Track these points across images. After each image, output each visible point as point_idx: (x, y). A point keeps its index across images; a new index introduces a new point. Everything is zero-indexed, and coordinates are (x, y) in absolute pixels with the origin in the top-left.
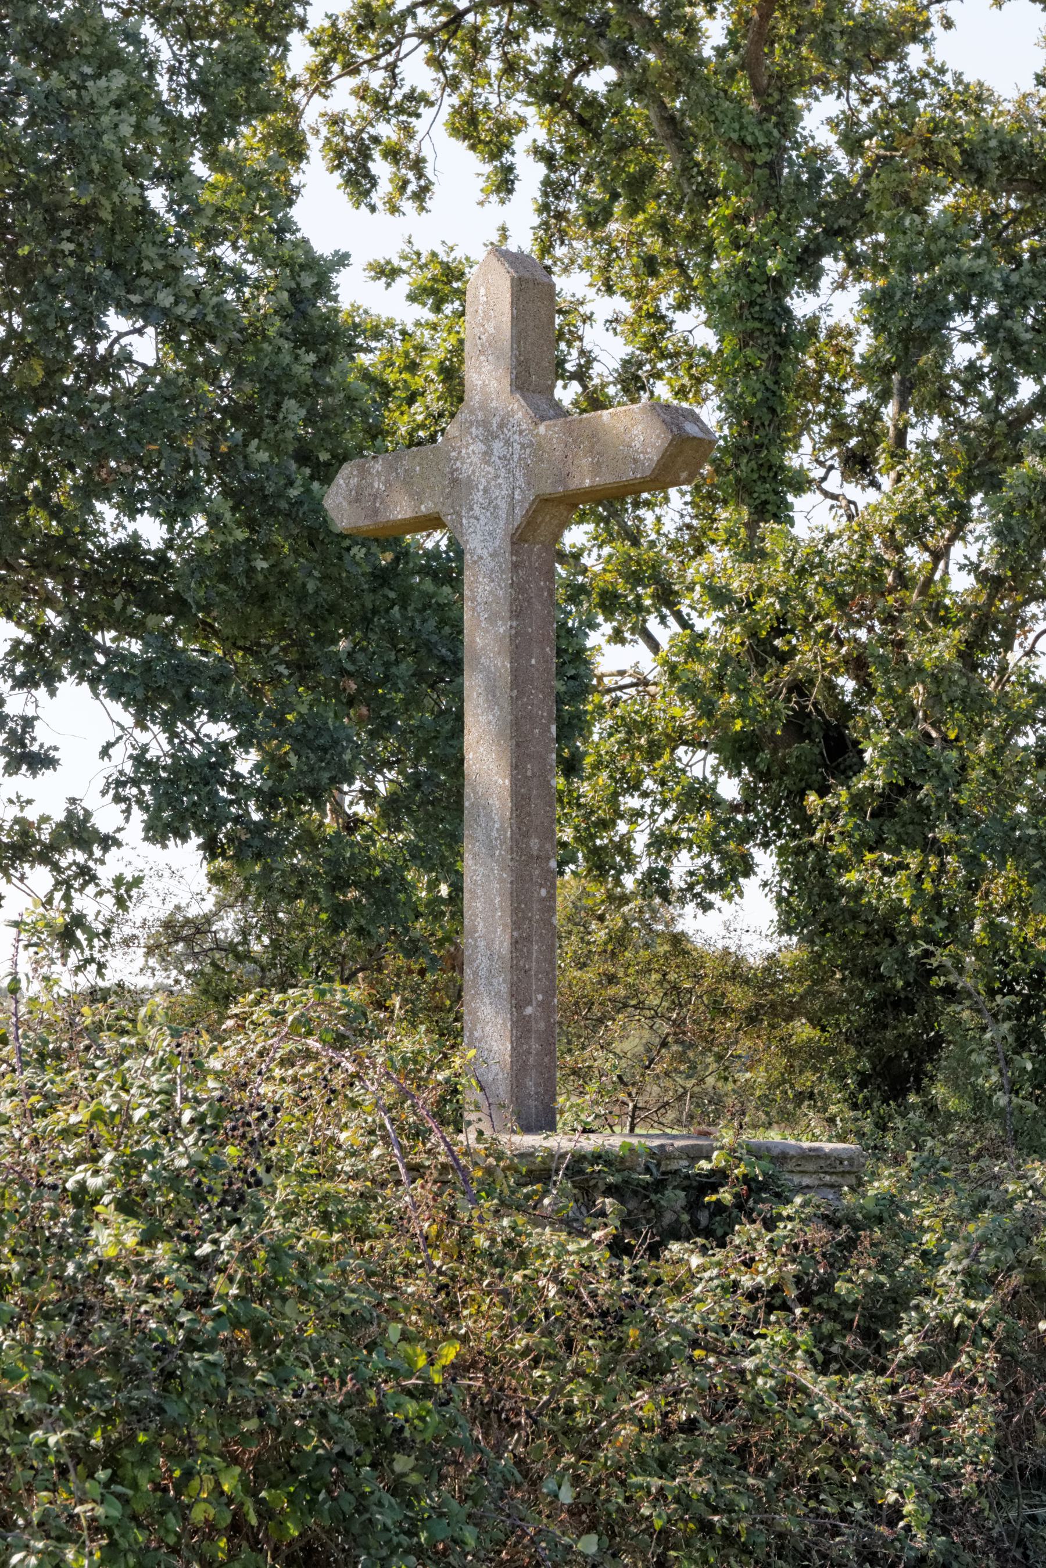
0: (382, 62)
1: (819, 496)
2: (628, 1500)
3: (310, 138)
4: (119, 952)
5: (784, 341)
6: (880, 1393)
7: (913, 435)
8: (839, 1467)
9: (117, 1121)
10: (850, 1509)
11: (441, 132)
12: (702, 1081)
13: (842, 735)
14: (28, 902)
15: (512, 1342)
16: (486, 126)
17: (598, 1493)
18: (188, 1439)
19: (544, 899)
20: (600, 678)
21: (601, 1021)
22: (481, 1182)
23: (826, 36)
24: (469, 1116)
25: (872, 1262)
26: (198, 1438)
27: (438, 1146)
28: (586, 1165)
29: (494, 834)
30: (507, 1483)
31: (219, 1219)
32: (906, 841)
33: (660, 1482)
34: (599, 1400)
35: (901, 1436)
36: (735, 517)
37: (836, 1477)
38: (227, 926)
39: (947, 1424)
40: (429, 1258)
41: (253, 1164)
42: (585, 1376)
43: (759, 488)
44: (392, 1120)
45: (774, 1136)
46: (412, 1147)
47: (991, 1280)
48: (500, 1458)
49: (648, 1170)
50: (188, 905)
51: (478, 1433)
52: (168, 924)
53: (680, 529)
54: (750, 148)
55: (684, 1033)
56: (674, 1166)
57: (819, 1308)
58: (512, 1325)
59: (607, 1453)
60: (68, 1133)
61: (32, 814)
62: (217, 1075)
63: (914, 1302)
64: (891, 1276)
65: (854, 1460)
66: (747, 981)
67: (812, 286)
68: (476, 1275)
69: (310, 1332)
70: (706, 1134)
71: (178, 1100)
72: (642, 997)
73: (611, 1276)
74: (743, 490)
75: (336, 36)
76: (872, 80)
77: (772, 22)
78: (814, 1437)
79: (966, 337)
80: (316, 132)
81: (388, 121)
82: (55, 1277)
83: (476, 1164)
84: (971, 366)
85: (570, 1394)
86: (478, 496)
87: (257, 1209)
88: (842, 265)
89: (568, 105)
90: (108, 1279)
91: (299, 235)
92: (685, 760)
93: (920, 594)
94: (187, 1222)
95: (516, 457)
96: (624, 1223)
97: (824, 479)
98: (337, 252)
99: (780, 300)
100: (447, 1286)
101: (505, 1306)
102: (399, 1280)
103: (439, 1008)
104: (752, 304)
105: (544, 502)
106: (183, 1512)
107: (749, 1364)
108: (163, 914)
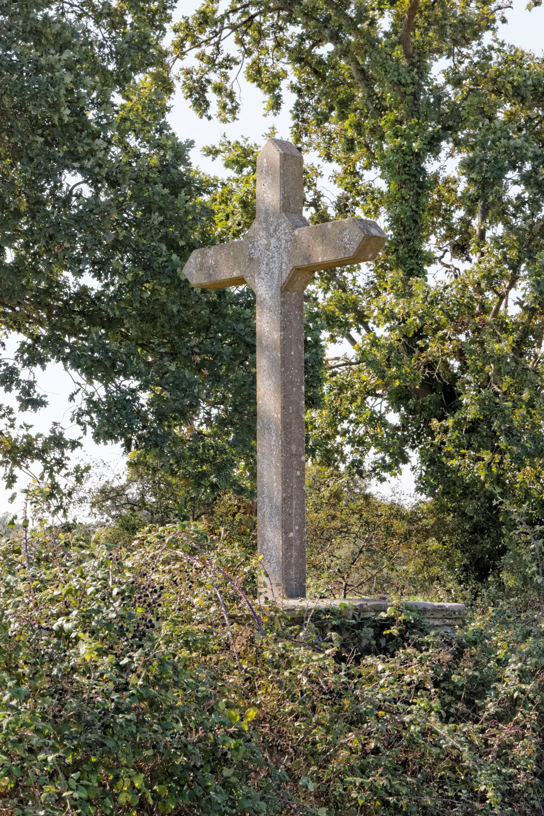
0: (212, 42)
1: (439, 266)
2: (345, 789)
3: (175, 82)
4: (77, 505)
5: (422, 186)
6: (476, 733)
7: (489, 234)
8: (455, 772)
9: (79, 594)
10: (460, 794)
11: (242, 77)
12: (381, 570)
13: (453, 390)
14: (30, 480)
15: (284, 708)
16: (265, 76)
17: (329, 786)
18: (117, 759)
19: (299, 477)
20: (327, 361)
21: (328, 540)
22: (267, 624)
23: (443, 27)
24: (260, 590)
25: (471, 664)
26: (122, 759)
27: (245, 605)
28: (321, 615)
29: (273, 443)
30: (282, 781)
31: (132, 645)
32: (482, 446)
33: (361, 780)
34: (329, 738)
35: (487, 755)
36: (396, 275)
37: (453, 776)
38: (133, 492)
39: (511, 749)
40: (241, 664)
41: (150, 616)
42: (322, 725)
43: (409, 262)
44: (221, 592)
45: (419, 600)
46: (231, 606)
47: (533, 674)
48: (278, 768)
49: (354, 618)
50: (113, 481)
51: (266, 755)
52: (102, 491)
53: (367, 284)
54: (403, 85)
55: (372, 546)
56: (367, 615)
57: (444, 688)
58: (284, 699)
59: (334, 766)
60: (53, 600)
61: (33, 433)
62: (130, 569)
63: (492, 686)
64: (481, 672)
65: (463, 768)
66: (403, 518)
67: (436, 157)
68: (265, 673)
69: (180, 703)
70: (384, 599)
71: (110, 583)
72: (349, 527)
73: (335, 673)
74: (400, 262)
75: (188, 27)
76: (465, 51)
77: (415, 20)
78: (442, 756)
79: (515, 183)
80: (179, 79)
81: (215, 72)
82: (47, 675)
83: (264, 615)
84: (519, 198)
85: (314, 735)
86: (264, 267)
87: (151, 640)
88: (451, 145)
89: (308, 64)
90: (74, 676)
91: (171, 131)
92: (371, 404)
93: (493, 316)
94: (115, 646)
95: (283, 247)
96: (342, 645)
97: (442, 257)
98: (187, 140)
99: (419, 164)
100: (250, 678)
101: (280, 689)
102: (225, 676)
103: (244, 534)
104: (405, 166)
105: (297, 270)
106: (115, 797)
107: (407, 718)
108: (100, 485)
